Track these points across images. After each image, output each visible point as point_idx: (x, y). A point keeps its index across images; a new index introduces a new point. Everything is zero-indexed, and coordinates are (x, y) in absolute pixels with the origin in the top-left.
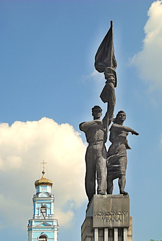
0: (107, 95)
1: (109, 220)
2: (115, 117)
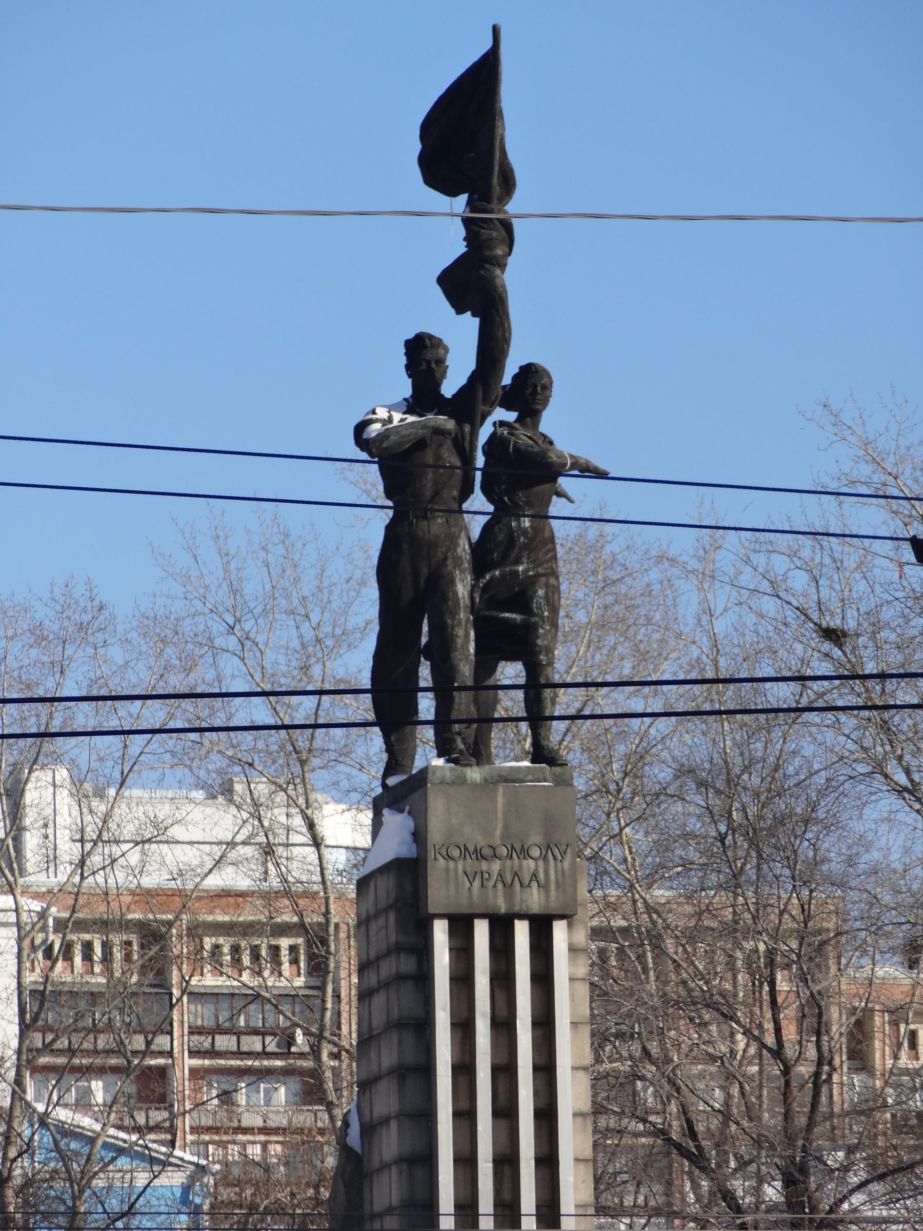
0: (472, 283)
1: (491, 883)
2: (507, 380)
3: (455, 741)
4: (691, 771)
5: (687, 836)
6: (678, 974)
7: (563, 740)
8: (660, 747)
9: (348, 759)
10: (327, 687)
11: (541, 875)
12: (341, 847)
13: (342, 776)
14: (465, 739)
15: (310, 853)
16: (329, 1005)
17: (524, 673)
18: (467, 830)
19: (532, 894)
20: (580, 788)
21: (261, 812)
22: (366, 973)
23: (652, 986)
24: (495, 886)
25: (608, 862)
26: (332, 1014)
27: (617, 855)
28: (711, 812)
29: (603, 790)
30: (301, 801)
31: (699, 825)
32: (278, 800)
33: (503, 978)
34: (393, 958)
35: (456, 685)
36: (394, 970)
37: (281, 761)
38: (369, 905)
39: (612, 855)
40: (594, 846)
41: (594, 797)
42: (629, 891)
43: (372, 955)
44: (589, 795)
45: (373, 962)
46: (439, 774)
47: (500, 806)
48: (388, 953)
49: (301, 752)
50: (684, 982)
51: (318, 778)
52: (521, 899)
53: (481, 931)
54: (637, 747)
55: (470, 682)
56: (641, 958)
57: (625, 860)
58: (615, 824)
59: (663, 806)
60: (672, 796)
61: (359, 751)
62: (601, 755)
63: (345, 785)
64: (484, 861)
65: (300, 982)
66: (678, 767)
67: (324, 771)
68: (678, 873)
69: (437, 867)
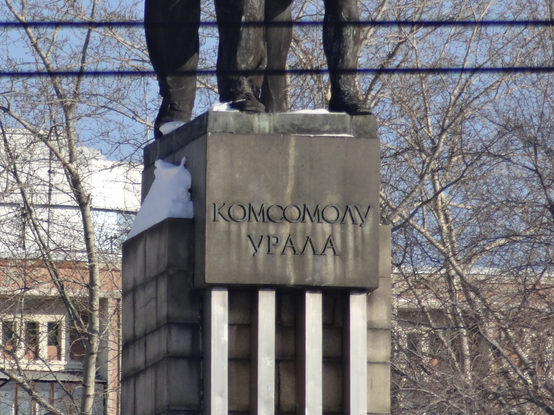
1: (279, 250)
3: (240, 83)
4: (519, 127)
5: (513, 203)
6: (498, 362)
7: (370, 89)
8: (482, 99)
9: (120, 106)
10: (97, 19)
11: (338, 241)
12: (112, 211)
13: (112, 126)
14: (252, 83)
15: (75, 217)
16: (91, 391)
17: (324, 12)
18: (252, 187)
19: (326, 263)
20: (389, 145)
21: (18, 166)
22: (131, 351)
23: (468, 378)
24: (283, 253)
25: (419, 231)
26: (95, 402)
27: (430, 223)
28: (540, 176)
29: (417, 147)
30: (64, 154)
31: (526, 191)
32: (37, 151)
33: (290, 360)
34: (164, 334)
35: (243, 18)
36: (164, 348)
37: (41, 107)
38: (136, 273)
39: (425, 224)
40: (404, 213)
41: (406, 156)
42: (445, 266)
43: (139, 330)
44: (400, 154)
45: (140, 338)
46: (221, 120)
47: (292, 161)
48: (158, 328)
49: (65, 96)
50: (505, 373)
51: (84, 127)
52: (314, 269)
53: (267, 304)
54: (457, 98)
55: (260, 16)
56: (456, 343)
57: (440, 230)
58: (429, 188)
59: (485, 168)
60: (496, 156)
61: (133, 96)
62: (415, 108)
63: (115, 135)
64: (271, 223)
65: (59, 365)
66: (503, 122)
67: (90, 119)
68: (500, 246)
69: (216, 230)
